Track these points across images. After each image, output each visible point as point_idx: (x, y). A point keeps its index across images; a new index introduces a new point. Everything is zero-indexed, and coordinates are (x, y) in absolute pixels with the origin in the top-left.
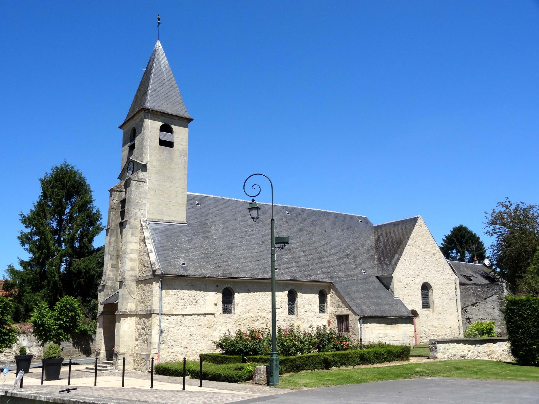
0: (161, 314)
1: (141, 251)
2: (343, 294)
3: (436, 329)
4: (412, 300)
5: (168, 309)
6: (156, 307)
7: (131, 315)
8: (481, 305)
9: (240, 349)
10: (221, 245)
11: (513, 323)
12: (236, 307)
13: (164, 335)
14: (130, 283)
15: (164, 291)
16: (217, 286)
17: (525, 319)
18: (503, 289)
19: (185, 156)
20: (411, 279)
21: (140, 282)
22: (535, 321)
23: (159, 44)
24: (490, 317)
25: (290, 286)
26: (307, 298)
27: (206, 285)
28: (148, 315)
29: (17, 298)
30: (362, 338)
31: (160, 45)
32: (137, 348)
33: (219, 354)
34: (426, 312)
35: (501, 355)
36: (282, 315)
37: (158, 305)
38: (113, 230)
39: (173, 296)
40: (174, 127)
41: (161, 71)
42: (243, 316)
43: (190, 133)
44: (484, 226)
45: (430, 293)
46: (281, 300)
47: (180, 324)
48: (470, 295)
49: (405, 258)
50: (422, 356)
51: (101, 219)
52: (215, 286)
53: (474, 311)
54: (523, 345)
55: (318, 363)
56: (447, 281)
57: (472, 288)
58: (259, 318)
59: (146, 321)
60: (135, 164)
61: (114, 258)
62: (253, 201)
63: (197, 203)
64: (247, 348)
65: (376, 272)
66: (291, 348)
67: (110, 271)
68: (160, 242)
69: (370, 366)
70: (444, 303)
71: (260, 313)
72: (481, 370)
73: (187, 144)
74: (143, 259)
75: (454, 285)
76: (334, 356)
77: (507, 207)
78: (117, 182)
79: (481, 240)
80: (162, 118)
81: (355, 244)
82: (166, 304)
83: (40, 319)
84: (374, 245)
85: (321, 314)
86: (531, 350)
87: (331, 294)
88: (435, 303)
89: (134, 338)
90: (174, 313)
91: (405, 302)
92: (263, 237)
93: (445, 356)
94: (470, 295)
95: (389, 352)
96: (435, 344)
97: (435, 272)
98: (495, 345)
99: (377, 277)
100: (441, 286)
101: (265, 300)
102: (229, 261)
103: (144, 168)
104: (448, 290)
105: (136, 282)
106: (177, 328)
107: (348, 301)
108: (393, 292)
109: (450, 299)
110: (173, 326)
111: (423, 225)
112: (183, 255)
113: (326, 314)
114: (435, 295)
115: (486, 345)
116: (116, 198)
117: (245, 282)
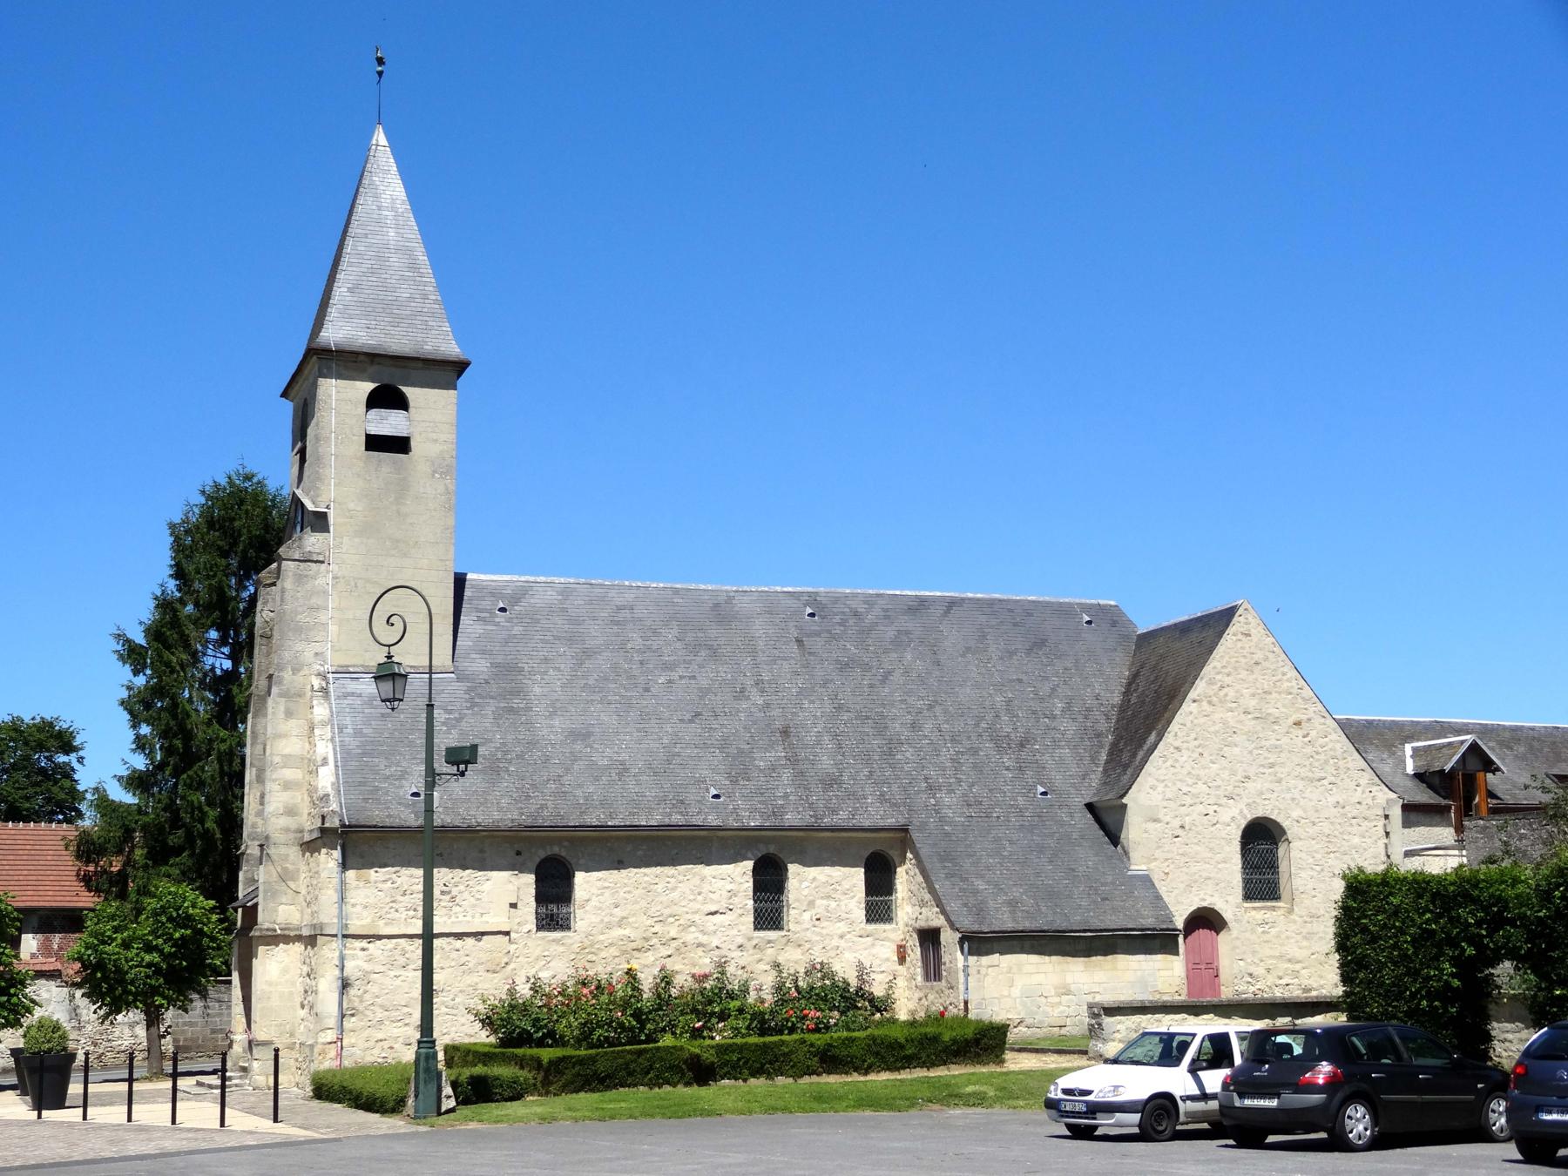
0: (345, 936)
3: (1298, 967)
5: (364, 922)
7: (287, 939)
10: (552, 729)
13: (352, 992)
14: (283, 850)
15: (351, 874)
16: (518, 853)
17: (1374, 939)
19: (446, 474)
20: (1201, 809)
23: (380, 137)
25: (761, 846)
26: (822, 878)
27: (482, 851)
29: (116, 884)
33: (485, 1045)
36: (735, 932)
37: (334, 910)
39: (380, 886)
40: (409, 391)
42: (601, 937)
43: (460, 404)
45: (1281, 851)
46: (730, 887)
47: (402, 961)
49: (1177, 744)
52: (513, 853)
55: (671, 1068)
56: (1351, 811)
62: (389, 657)
64: (541, 1028)
68: (358, 733)
71: (657, 928)
73: (452, 437)
75: (1383, 821)
80: (372, 369)
81: (1042, 699)
83: (94, 948)
85: (872, 927)
87: (908, 865)
88: (1297, 883)
92: (701, 698)
96: (1098, 1015)
97: (1301, 784)
99: (1090, 807)
100: (1326, 828)
101: (674, 889)
103: (320, 522)
106: (392, 973)
108: (1126, 853)
110: (382, 969)
111: (1257, 631)
117: (607, 839)
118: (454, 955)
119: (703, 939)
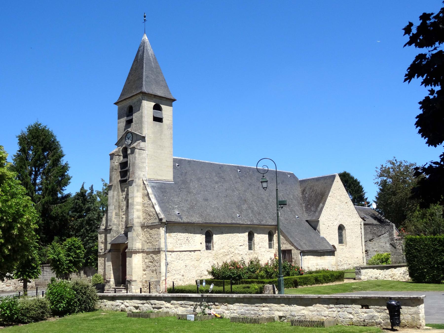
1: (145, 204)
2: (287, 234)
4: (332, 238)
6: (163, 246)
7: (139, 252)
8: (376, 240)
9: (230, 275)
11: (411, 254)
12: (214, 245)
13: (169, 266)
15: (167, 234)
17: (419, 251)
18: (393, 228)
20: (331, 222)
21: (143, 227)
22: (426, 253)
24: (383, 250)
26: (261, 237)
27: (194, 229)
28: (158, 252)
30: (302, 266)
31: (147, 38)
32: (145, 276)
34: (341, 247)
35: (399, 277)
38: (115, 186)
39: (174, 238)
40: (163, 106)
41: (150, 60)
44: (374, 178)
45: (343, 232)
46: (244, 239)
47: (179, 258)
48: (368, 233)
50: (349, 278)
51: (68, 170)
53: (371, 245)
54: (417, 269)
55: (291, 283)
57: (369, 228)
58: (229, 253)
59: (154, 256)
60: (133, 135)
61: (117, 208)
63: (177, 165)
64: (234, 274)
65: (307, 217)
66: (273, 273)
67: (115, 218)
68: (159, 196)
69: (321, 285)
70: (353, 240)
71: (230, 249)
72: (394, 286)
74: (147, 209)
76: (300, 278)
77: (393, 164)
78: (115, 149)
79: (361, 184)
80: (154, 99)
82: (169, 244)
84: (301, 196)
85: (270, 249)
86: (423, 272)
88: (347, 239)
89: (142, 269)
90: (175, 250)
91: (328, 239)
93: (366, 278)
94: (368, 233)
95: (332, 275)
96: (359, 269)
98: (396, 270)
99: (307, 221)
102: (208, 211)
103: (143, 139)
104: (356, 230)
105: (142, 227)
106: (177, 261)
107: (291, 239)
108: (319, 232)
109: (357, 237)
112: (176, 207)
113: (272, 249)
114: (347, 233)
115: (390, 270)
116: (117, 161)
117: (220, 226)
118: (190, 256)
119: (239, 252)
